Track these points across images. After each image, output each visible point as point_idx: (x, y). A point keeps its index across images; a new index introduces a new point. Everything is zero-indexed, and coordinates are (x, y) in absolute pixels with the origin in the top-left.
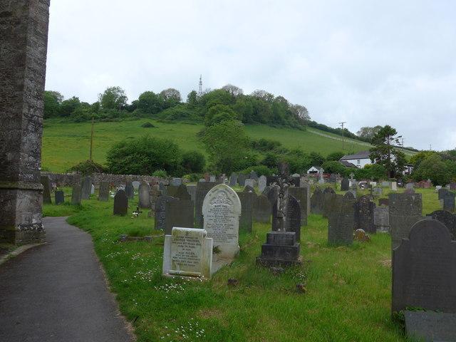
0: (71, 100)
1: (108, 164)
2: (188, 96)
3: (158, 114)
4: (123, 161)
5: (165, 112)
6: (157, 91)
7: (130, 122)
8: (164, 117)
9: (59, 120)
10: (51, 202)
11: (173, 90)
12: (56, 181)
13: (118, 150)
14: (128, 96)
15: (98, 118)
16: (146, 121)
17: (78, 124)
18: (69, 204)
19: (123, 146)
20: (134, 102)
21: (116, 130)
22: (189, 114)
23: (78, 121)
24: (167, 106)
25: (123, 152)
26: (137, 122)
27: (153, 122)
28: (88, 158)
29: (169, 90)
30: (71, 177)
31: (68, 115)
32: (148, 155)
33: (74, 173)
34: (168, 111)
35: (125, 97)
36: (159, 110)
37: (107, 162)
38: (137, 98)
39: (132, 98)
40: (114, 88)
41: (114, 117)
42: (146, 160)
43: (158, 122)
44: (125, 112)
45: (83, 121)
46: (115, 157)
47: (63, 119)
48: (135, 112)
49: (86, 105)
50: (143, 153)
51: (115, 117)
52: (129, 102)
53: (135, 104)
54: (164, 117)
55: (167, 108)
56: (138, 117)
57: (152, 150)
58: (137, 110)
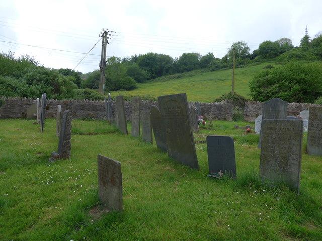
0: (208, 55)
1: (251, 95)
2: (301, 41)
3: (277, 57)
4: (269, 90)
5: (282, 56)
6: (273, 40)
7: (254, 66)
8: (282, 59)
9: (200, 71)
10: (195, 165)
11: (286, 39)
12: (202, 113)
13: (261, 80)
14: (249, 45)
15: (227, 67)
16: (266, 64)
17: (213, 72)
18: (258, 187)
19: (266, 76)
20: (255, 52)
21: (243, 73)
22: (304, 55)
23: (213, 70)
24: (282, 51)
25: (267, 80)
26: (259, 66)
27: (272, 65)
28: (231, 91)
29: (282, 40)
30: (219, 108)
31: (206, 67)
32: (299, 82)
33: (222, 102)
34: (285, 54)
35: (247, 48)
36: (276, 55)
37: (250, 93)
38: (257, 47)
39: (253, 47)
40: (239, 43)
41: (240, 64)
42: (296, 87)
43: (276, 64)
44: (248, 60)
45: (217, 70)
46: (259, 87)
47: (203, 70)
48: (256, 58)
49: (218, 59)
50: (291, 80)
51: (240, 64)
52: (251, 52)
53: (256, 53)
54: (282, 59)
55: (283, 52)
56: (259, 62)
57: (303, 76)
58: (258, 56)
